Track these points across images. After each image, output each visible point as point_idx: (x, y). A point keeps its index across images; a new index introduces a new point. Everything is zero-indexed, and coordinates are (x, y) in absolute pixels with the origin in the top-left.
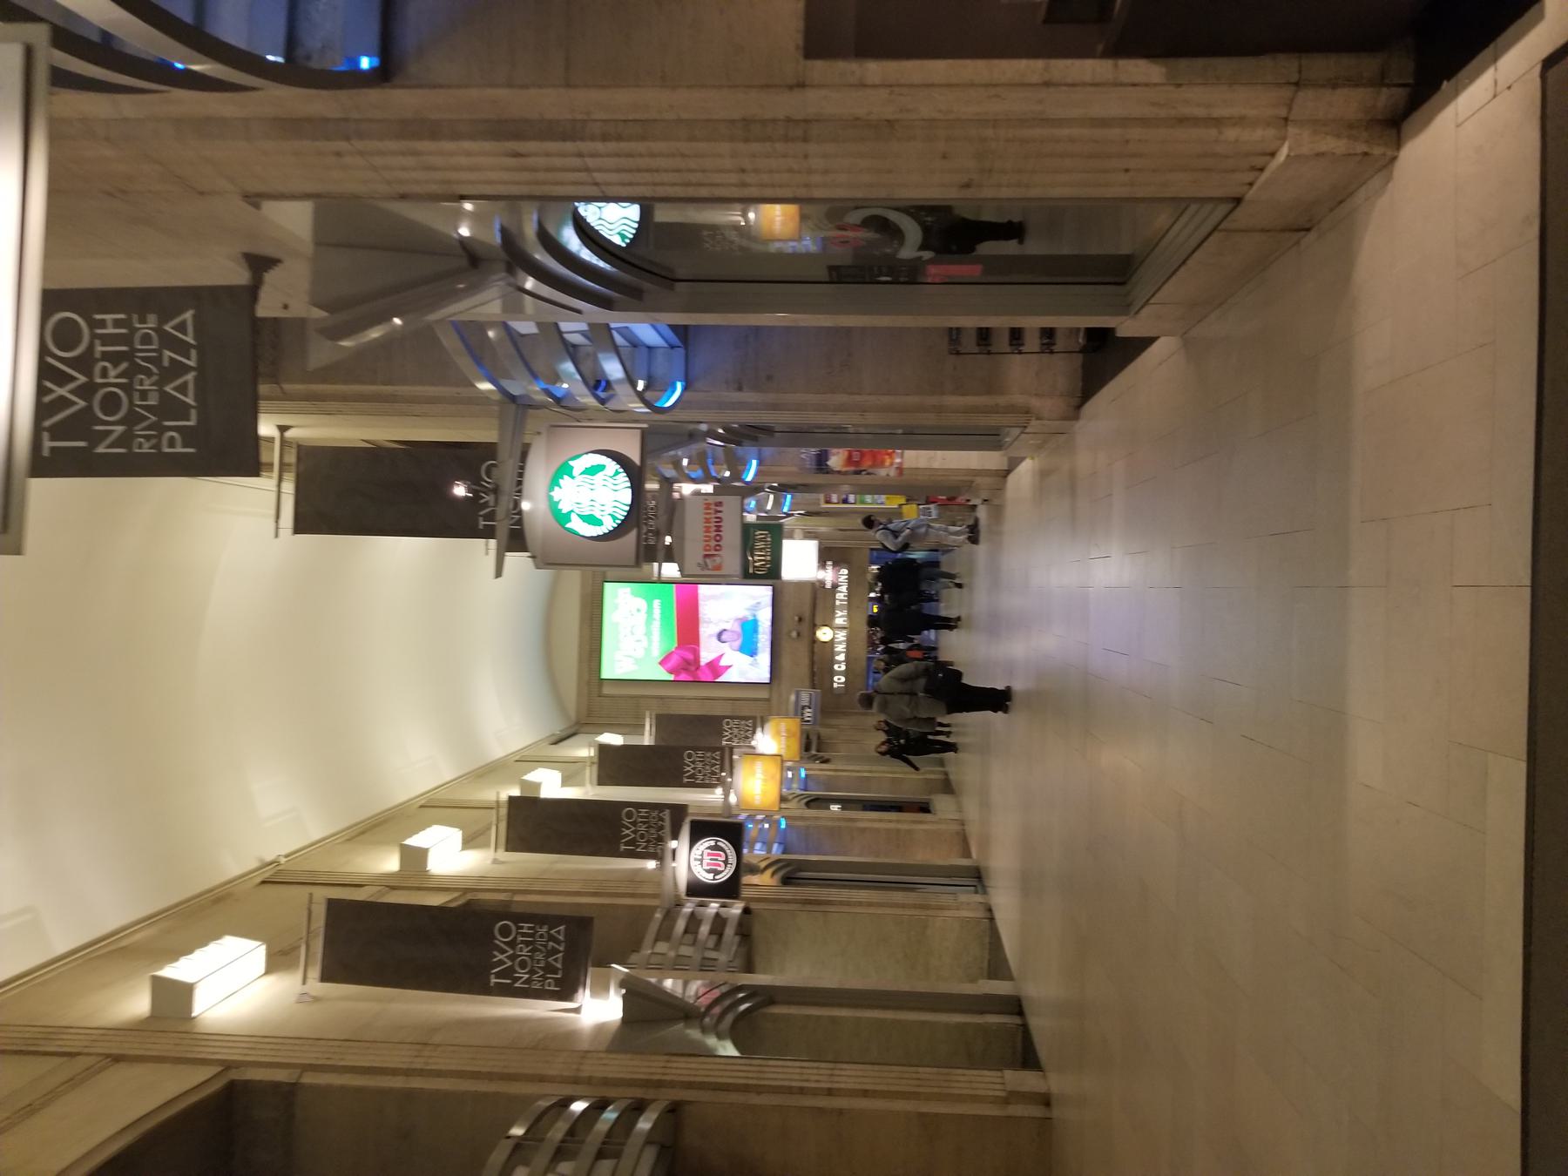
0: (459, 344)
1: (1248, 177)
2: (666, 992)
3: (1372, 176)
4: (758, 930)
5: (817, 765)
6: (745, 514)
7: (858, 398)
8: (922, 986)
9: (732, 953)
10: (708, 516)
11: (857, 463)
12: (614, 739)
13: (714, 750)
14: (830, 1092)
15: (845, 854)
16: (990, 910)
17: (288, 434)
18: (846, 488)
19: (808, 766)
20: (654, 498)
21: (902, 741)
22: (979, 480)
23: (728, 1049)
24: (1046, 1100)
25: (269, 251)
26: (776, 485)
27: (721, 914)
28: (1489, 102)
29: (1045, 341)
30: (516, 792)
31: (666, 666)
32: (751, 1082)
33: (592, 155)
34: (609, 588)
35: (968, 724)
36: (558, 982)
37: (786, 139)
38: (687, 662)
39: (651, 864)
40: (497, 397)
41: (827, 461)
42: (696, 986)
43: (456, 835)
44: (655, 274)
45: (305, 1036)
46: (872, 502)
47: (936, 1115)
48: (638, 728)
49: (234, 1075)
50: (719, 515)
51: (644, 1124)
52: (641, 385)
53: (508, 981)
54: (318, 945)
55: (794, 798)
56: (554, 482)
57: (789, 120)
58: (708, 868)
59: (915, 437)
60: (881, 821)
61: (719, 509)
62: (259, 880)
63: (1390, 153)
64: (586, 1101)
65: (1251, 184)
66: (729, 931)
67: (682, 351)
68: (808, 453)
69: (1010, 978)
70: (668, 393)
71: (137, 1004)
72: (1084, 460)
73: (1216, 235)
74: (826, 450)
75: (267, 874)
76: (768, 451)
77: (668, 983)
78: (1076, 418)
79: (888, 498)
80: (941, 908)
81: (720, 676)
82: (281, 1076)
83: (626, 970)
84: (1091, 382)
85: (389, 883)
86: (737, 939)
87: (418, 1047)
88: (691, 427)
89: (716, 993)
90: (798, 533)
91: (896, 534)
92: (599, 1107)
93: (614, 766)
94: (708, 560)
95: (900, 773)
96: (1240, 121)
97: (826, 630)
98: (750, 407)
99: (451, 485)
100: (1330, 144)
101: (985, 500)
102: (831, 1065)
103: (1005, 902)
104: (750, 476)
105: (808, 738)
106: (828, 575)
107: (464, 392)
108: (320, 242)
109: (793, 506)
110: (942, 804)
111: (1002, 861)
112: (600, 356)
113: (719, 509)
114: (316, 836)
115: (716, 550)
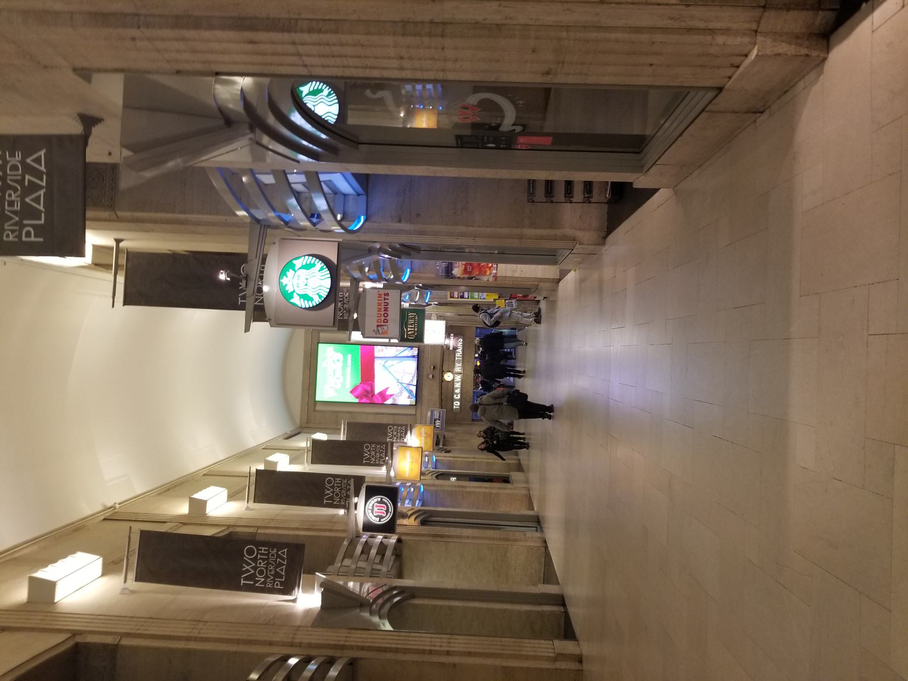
0: (224, 186)
1: (728, 72)
2: (349, 590)
3: (808, 73)
4: (406, 553)
5: (443, 454)
6: (402, 303)
7: (471, 229)
8: (504, 588)
9: (390, 566)
10: (380, 302)
11: (470, 273)
12: (321, 436)
13: (381, 444)
14: (448, 653)
15: (458, 507)
16: (545, 542)
17: (122, 245)
18: (463, 288)
19: (439, 454)
20: (348, 291)
21: (495, 442)
22: (542, 284)
23: (388, 627)
24: (580, 659)
25: (94, 112)
26: (421, 285)
27: (384, 543)
28: (898, 11)
29: (586, 196)
30: (261, 467)
31: (355, 394)
32: (399, 646)
33: (302, 44)
34: (321, 347)
35: (532, 427)
36: (282, 583)
37: (430, 35)
38: (367, 391)
39: (342, 512)
40: (248, 220)
41: (452, 271)
42: (367, 586)
43: (223, 493)
44: (349, 140)
45: (123, 615)
46: (478, 297)
47: (513, 668)
48: (337, 430)
49: (78, 639)
50: (386, 301)
51: (333, 673)
52: (339, 217)
53: (252, 583)
54: (134, 559)
55: (429, 473)
56: (283, 273)
57: (432, 22)
58: (376, 515)
59: (506, 255)
60: (480, 487)
61: (386, 297)
62: (102, 518)
63: (822, 55)
64: (298, 658)
65: (730, 78)
66: (389, 553)
67: (364, 197)
68: (440, 265)
69: (558, 583)
70: (355, 223)
71: (20, 594)
72: (608, 273)
73: (704, 114)
74: (451, 263)
75: (107, 514)
76: (417, 262)
77: (351, 584)
78: (604, 244)
79: (488, 295)
80: (516, 540)
81: (386, 400)
82: (109, 640)
83: (324, 577)
84: (612, 223)
85: (183, 521)
86: (393, 557)
87: (194, 623)
88: (371, 245)
89: (380, 591)
90: (434, 316)
91: (491, 315)
92: (305, 661)
93: (321, 452)
94: (379, 328)
95: (492, 459)
96: (726, 31)
97: (450, 374)
98: (406, 232)
99: (218, 273)
100: (786, 48)
101: (545, 298)
102: (449, 636)
103: (554, 537)
104: (405, 279)
105: (438, 437)
106: (451, 342)
107: (230, 219)
108: (127, 105)
109: (431, 299)
110: (515, 476)
111: (553, 513)
112: (313, 195)
113: (386, 297)
114: (139, 492)
115: (384, 322)
